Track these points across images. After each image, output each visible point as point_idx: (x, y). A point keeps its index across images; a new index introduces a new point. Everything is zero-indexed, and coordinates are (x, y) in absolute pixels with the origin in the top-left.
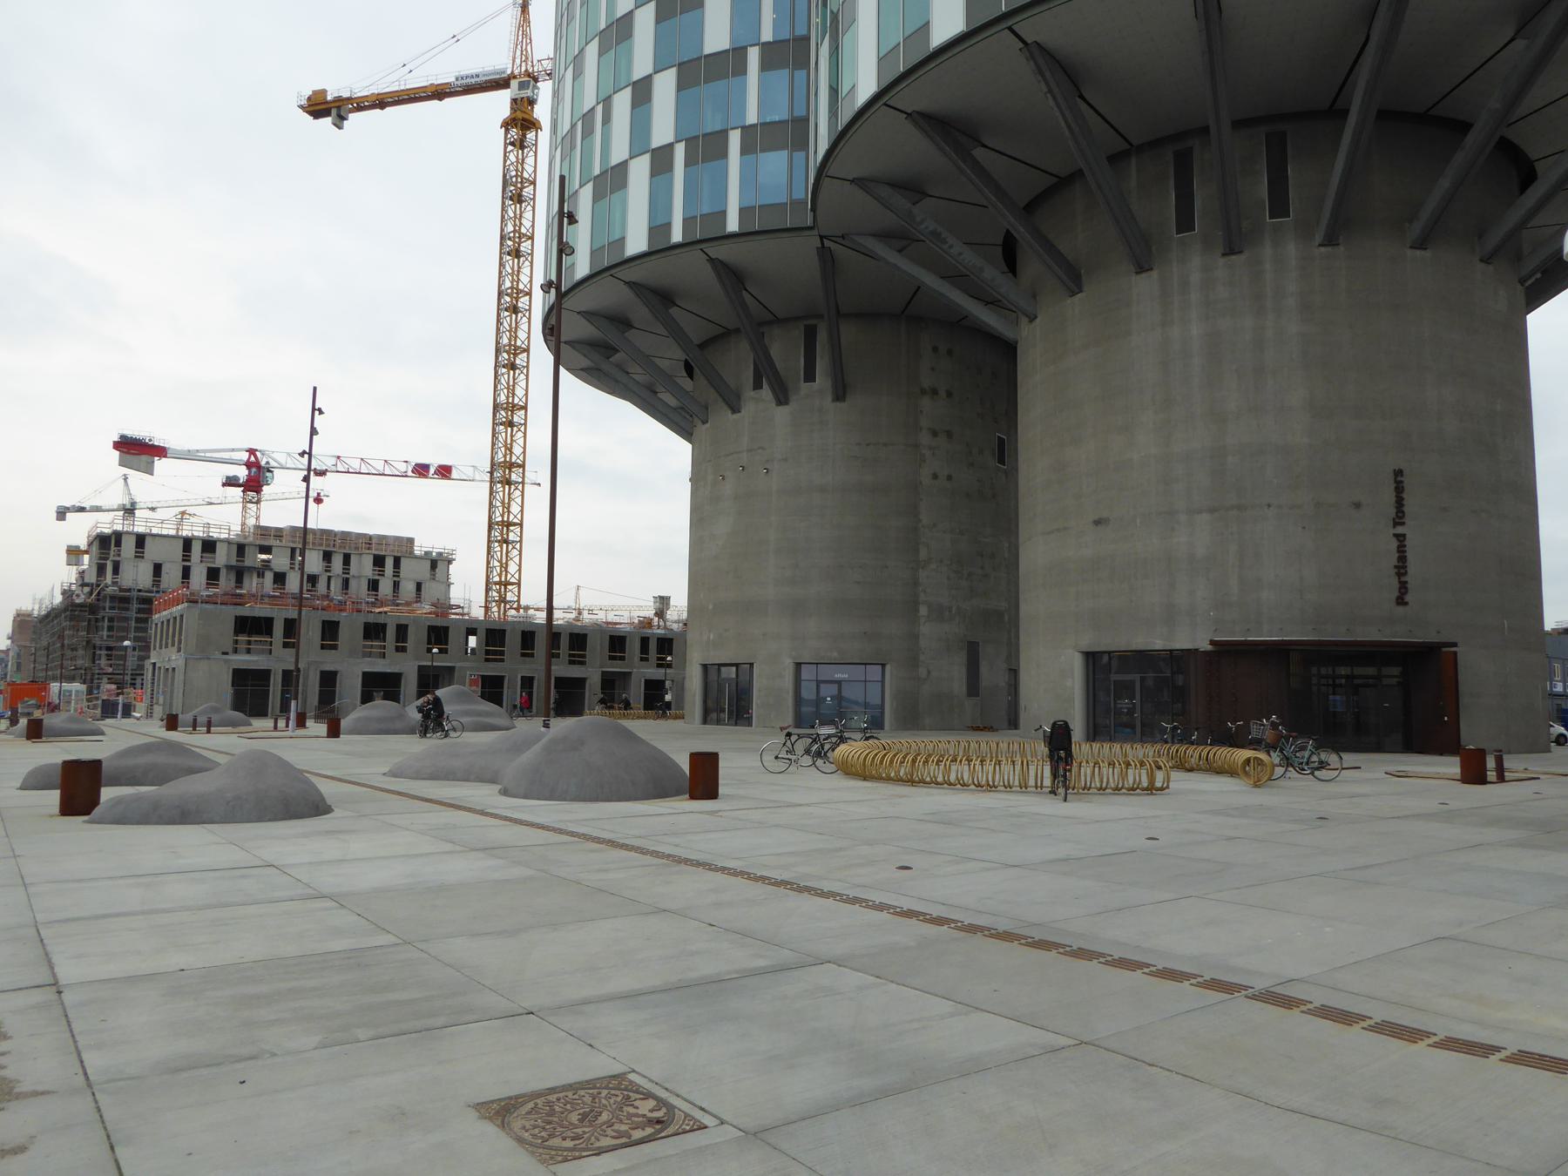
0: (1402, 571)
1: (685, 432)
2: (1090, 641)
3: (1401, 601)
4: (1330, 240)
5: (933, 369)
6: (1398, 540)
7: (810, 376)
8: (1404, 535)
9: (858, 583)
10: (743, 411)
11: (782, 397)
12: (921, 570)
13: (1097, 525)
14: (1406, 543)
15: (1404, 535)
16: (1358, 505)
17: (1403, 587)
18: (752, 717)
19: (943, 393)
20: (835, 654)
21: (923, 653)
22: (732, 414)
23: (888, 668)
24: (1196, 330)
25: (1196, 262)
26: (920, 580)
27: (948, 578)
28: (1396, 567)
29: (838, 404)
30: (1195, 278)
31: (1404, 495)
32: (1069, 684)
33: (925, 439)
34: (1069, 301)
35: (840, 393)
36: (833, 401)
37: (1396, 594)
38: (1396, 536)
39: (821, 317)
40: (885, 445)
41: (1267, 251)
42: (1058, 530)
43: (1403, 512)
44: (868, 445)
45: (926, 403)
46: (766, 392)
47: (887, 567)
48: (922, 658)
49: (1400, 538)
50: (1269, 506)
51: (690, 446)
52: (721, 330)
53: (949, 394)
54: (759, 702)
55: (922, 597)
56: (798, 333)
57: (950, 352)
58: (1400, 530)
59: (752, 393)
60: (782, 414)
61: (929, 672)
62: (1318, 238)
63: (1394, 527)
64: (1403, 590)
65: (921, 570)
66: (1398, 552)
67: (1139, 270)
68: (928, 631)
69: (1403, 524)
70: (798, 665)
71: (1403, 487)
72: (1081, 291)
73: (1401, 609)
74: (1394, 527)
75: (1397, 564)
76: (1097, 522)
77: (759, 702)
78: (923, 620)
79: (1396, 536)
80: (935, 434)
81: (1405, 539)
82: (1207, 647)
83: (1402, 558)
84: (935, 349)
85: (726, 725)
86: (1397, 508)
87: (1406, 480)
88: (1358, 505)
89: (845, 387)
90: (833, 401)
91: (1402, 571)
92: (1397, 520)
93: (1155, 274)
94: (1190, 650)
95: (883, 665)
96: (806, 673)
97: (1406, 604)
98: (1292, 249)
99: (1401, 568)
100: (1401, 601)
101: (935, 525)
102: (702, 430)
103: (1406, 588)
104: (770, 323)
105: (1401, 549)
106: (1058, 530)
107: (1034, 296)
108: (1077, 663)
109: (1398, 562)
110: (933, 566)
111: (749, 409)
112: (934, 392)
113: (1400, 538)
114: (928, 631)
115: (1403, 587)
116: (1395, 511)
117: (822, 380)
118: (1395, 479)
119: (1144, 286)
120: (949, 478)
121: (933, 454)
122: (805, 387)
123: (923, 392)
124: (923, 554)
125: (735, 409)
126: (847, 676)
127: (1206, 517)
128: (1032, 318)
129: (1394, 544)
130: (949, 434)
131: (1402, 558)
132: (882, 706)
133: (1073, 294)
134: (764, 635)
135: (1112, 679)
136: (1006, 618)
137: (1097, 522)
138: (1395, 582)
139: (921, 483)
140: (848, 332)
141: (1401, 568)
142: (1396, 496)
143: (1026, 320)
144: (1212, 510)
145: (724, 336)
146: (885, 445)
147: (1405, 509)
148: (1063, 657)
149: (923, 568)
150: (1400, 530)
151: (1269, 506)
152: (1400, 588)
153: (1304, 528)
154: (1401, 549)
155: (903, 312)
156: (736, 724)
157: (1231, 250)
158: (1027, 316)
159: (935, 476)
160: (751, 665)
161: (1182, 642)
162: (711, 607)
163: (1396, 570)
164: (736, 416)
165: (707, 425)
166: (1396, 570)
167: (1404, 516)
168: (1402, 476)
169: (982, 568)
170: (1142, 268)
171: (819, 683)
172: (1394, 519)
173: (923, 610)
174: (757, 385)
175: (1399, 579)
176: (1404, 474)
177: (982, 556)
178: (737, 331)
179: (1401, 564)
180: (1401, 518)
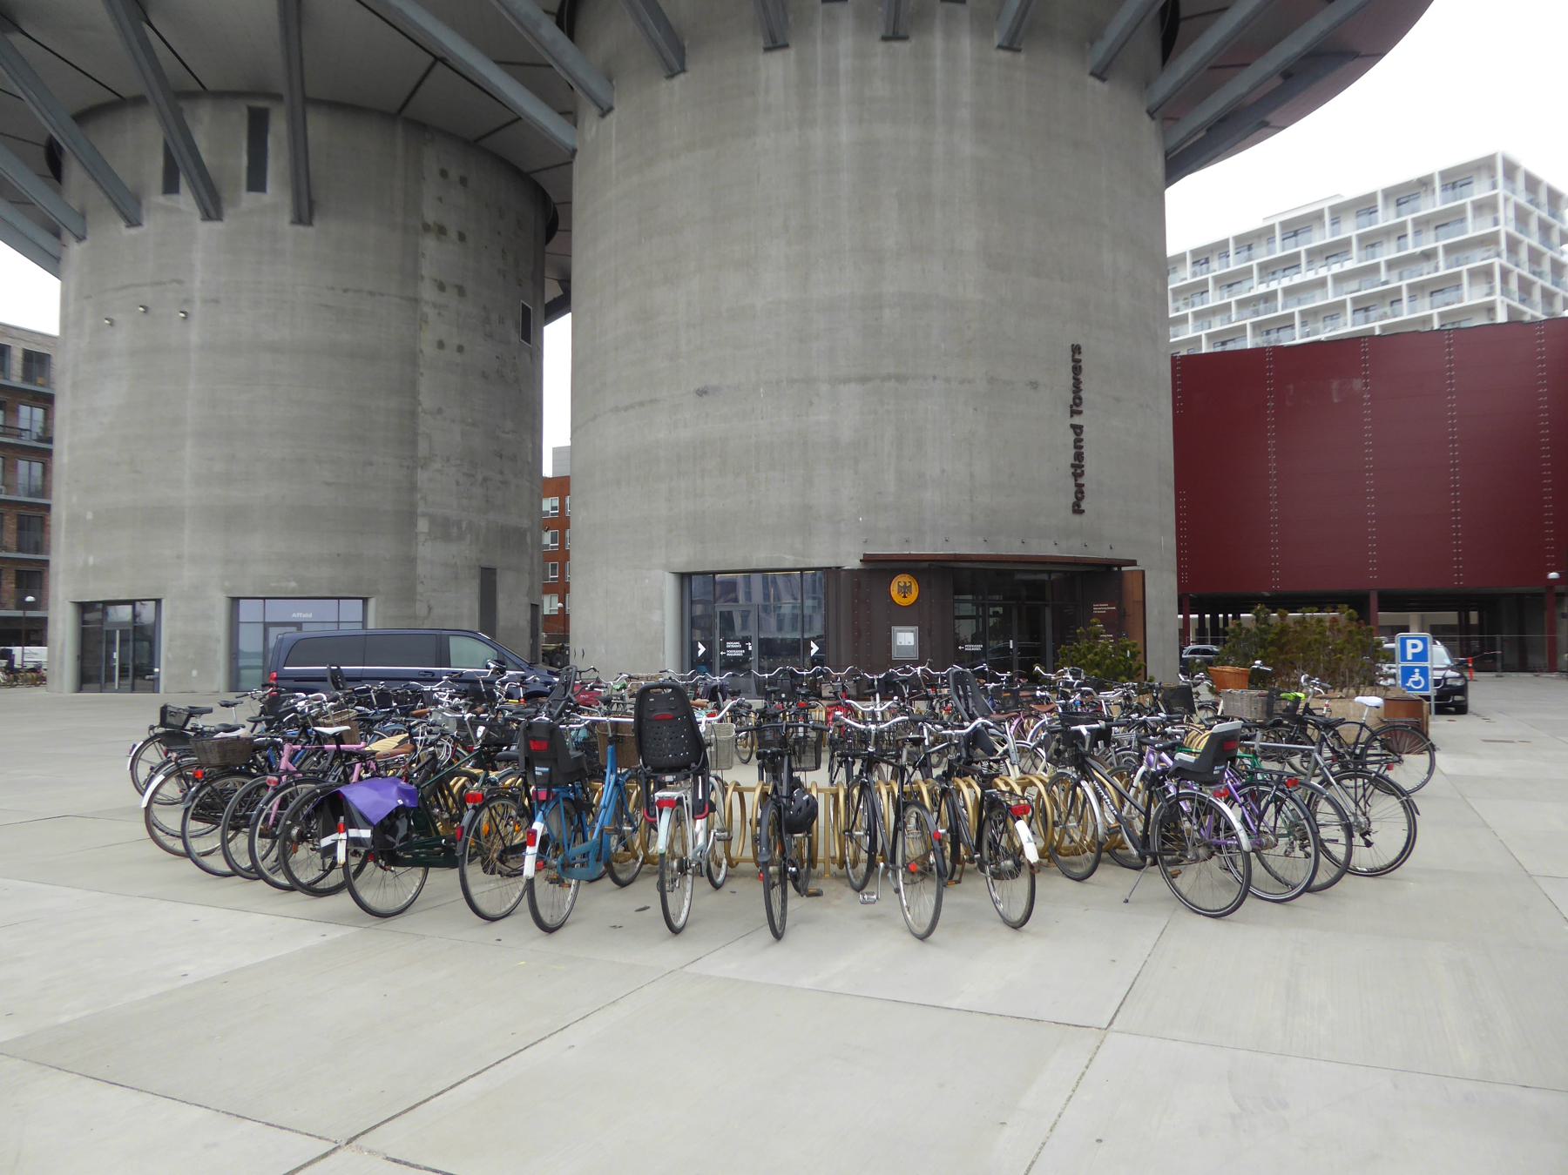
0: (1079, 471)
1: (51, 262)
2: (686, 559)
3: (1077, 509)
4: (1011, 45)
5: (440, 199)
6: (1076, 433)
7: (257, 181)
8: (1081, 427)
9: (328, 484)
10: (145, 223)
11: (212, 208)
12: (419, 470)
13: (701, 396)
14: (1082, 437)
15: (1081, 427)
16: (1034, 385)
17: (1080, 490)
18: (158, 679)
19: (453, 235)
20: (293, 584)
21: (422, 582)
22: (127, 227)
23: (372, 603)
24: (846, 134)
25: (846, 43)
26: (419, 483)
27: (458, 483)
28: (1073, 466)
29: (301, 229)
30: (845, 64)
31: (1082, 377)
32: (656, 617)
33: (428, 292)
34: (664, 84)
35: (304, 212)
36: (293, 222)
37: (1072, 499)
38: (1074, 427)
39: (277, 97)
40: (371, 293)
41: (938, 42)
42: (641, 404)
43: (1080, 399)
44: (346, 291)
45: (429, 243)
46: (185, 200)
47: (371, 464)
48: (420, 588)
49: (1077, 429)
50: (935, 378)
51: (59, 282)
52: (110, 97)
53: (462, 237)
54: (170, 656)
55: (421, 509)
56: (237, 119)
57: (463, 181)
58: (1077, 420)
59: (161, 199)
60: (205, 230)
61: (430, 609)
62: (997, 40)
63: (1072, 416)
64: (1080, 496)
65: (419, 470)
66: (1076, 447)
67: (770, 45)
68: (430, 554)
69: (1080, 413)
70: (235, 601)
71: (1080, 367)
72: (683, 70)
73: (1077, 518)
74: (1072, 416)
75: (1073, 462)
76: (702, 393)
77: (170, 656)
78: (421, 538)
79: (1074, 427)
80: (442, 287)
81: (1082, 432)
82: (853, 563)
83: (1079, 456)
84: (444, 174)
85: (116, 692)
86: (1074, 392)
87: (1084, 357)
88: (1034, 385)
89: (311, 203)
90: (293, 222)
91: (1079, 471)
92: (1075, 408)
93: (791, 53)
94: (830, 568)
95: (365, 600)
96: (249, 611)
97: (1084, 511)
98: (966, 45)
99: (1078, 469)
100: (1077, 509)
101: (440, 411)
102: (75, 251)
103: (1082, 492)
104: (190, 96)
105: (1078, 444)
106: (641, 404)
107: (610, 81)
108: (669, 586)
109: (1075, 460)
110: (437, 465)
111: (151, 225)
112: (441, 231)
113: (1077, 429)
114: (430, 554)
115: (1080, 490)
116: (1072, 396)
117: (277, 192)
118: (1073, 356)
119: (776, 68)
120: (460, 349)
121: (439, 314)
122: (248, 199)
123: (426, 228)
124: (423, 448)
125: (133, 222)
126: (310, 616)
127: (854, 387)
128: (605, 111)
129: (1071, 437)
130: (461, 291)
131: (1079, 456)
132: (663, 624)
133: (672, 75)
134: (179, 557)
135: (718, 610)
136: (529, 539)
137: (702, 393)
138: (1070, 483)
139: (421, 351)
140: (318, 126)
141: (1078, 469)
142: (1074, 378)
143: (595, 111)
144: (863, 380)
145: (117, 105)
146: (371, 293)
147: (1083, 395)
148: (647, 581)
149: (422, 467)
150: (1077, 420)
151: (935, 378)
152: (1076, 493)
153: (975, 409)
154: (1078, 444)
155: (400, 111)
156: (133, 690)
157: (894, 35)
158: (599, 106)
159: (441, 345)
160: (158, 601)
161: (822, 557)
162: (90, 516)
163: (1073, 470)
164: (133, 231)
165: (85, 244)
166: (1073, 470)
167: (1081, 403)
168: (1080, 353)
169: (501, 473)
170: (775, 44)
171: (267, 626)
172: (1071, 406)
173: (423, 525)
174: (171, 187)
175: (1076, 480)
176: (1082, 350)
177: (501, 456)
178: (139, 101)
179: (1077, 462)
180: (1077, 405)
